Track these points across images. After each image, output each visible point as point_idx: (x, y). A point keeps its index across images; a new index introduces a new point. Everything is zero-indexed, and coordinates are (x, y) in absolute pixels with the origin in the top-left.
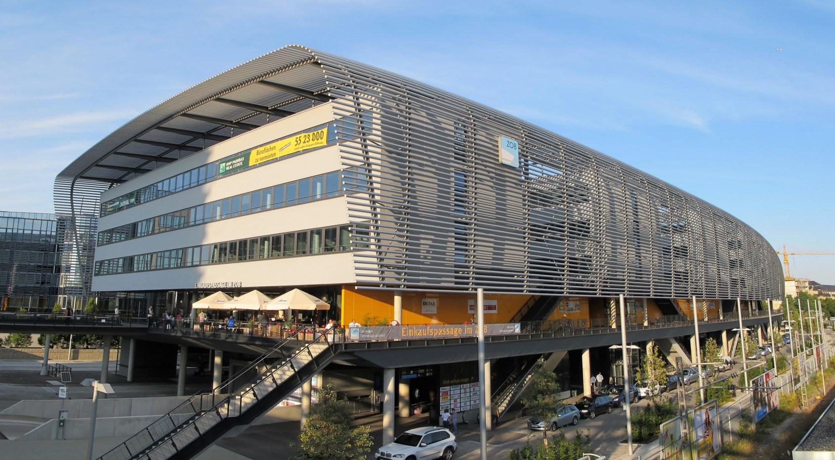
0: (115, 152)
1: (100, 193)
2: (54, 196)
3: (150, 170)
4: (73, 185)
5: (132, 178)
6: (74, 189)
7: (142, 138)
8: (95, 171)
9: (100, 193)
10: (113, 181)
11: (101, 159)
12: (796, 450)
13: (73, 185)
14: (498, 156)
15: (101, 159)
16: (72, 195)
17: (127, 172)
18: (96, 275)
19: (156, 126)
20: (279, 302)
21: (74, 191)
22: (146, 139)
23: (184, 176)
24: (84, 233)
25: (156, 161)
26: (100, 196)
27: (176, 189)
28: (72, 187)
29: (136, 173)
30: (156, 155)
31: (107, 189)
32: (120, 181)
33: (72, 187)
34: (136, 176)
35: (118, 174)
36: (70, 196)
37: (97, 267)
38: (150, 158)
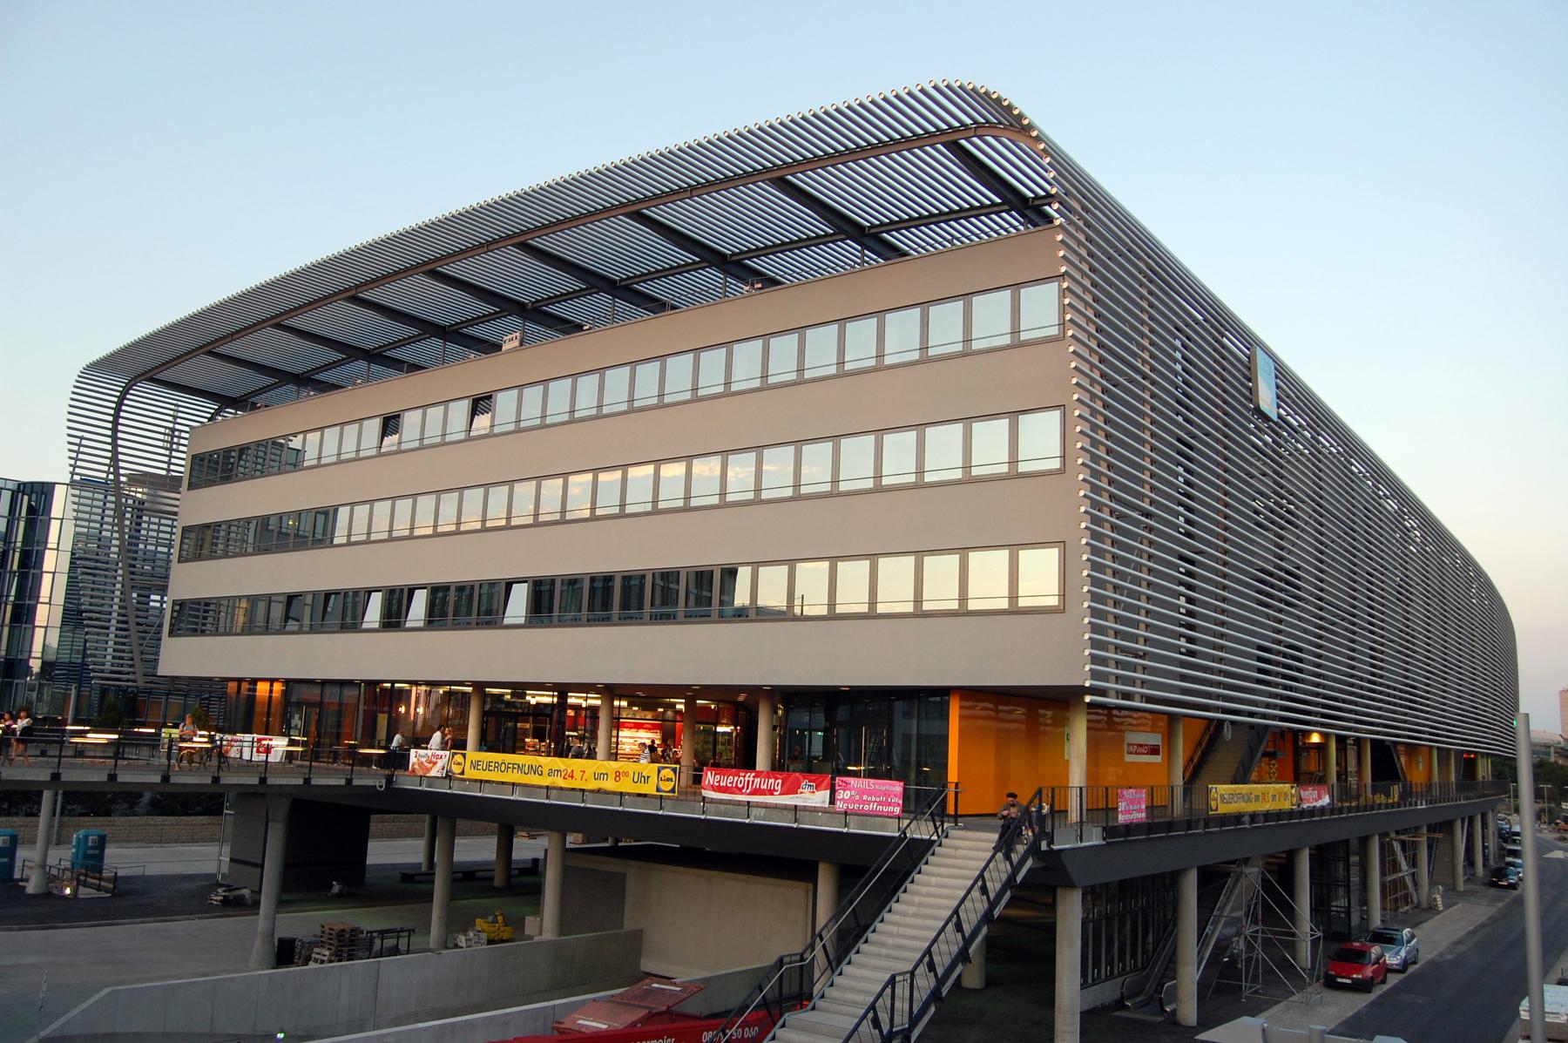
0: (210, 350)
1: (187, 429)
2: (69, 420)
3: (341, 387)
4: (122, 398)
5: (706, 297)
6: (114, 405)
7: (228, 349)
8: (206, 371)
10: (225, 401)
13: (122, 398)
14: (76, 526)
16: (115, 423)
18: (171, 633)
19: (145, 377)
20: (821, 992)
22: (238, 355)
23: (322, 435)
24: (86, 530)
25: (525, 318)
27: (444, 435)
28: (120, 404)
29: (445, 340)
30: (367, 347)
31: (206, 420)
32: (242, 403)
33: (120, 404)
34: (368, 379)
35: (243, 381)
36: (111, 418)
37: (245, 686)
38: (284, 377)
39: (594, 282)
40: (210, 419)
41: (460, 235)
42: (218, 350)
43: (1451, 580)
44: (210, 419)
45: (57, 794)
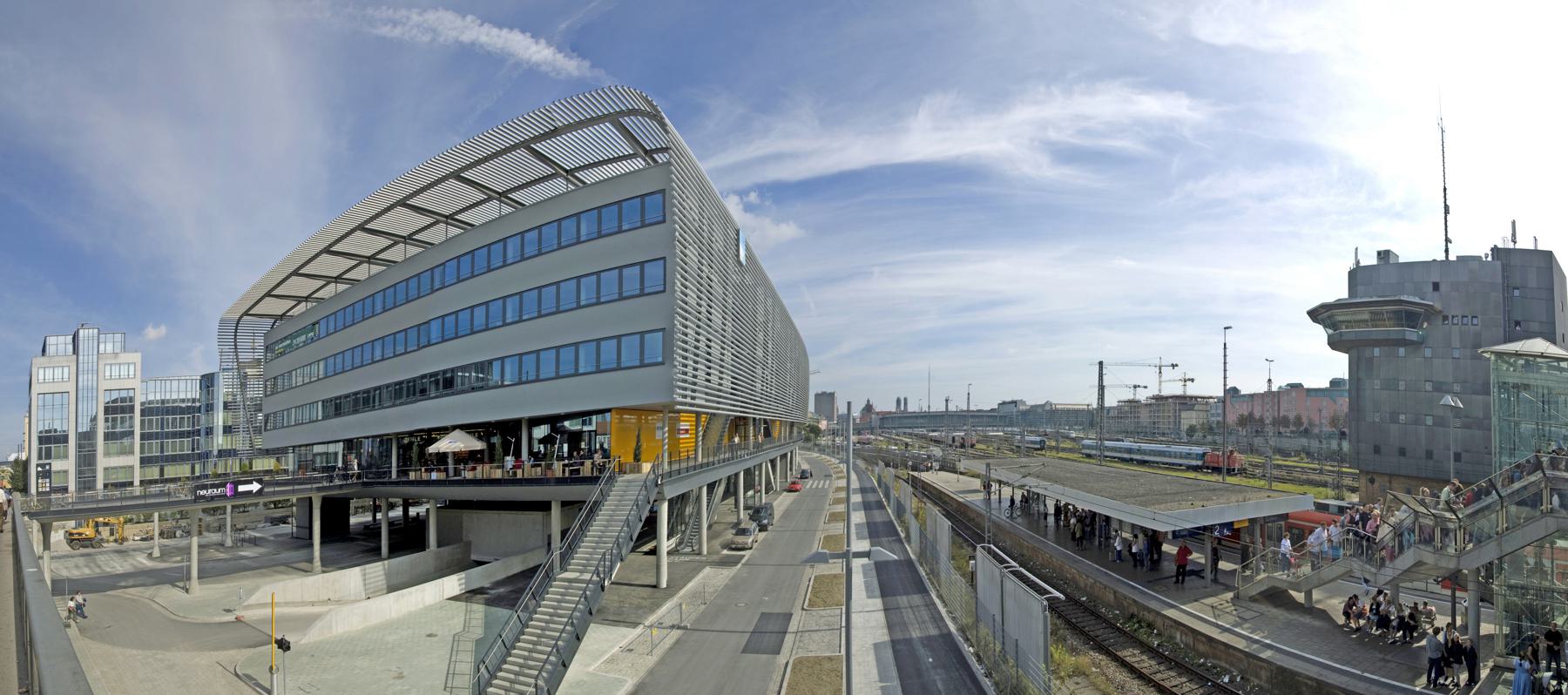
11: (278, 285)
15: (278, 285)
30: (335, 275)
41: (692, 190)
45: (157, 403)
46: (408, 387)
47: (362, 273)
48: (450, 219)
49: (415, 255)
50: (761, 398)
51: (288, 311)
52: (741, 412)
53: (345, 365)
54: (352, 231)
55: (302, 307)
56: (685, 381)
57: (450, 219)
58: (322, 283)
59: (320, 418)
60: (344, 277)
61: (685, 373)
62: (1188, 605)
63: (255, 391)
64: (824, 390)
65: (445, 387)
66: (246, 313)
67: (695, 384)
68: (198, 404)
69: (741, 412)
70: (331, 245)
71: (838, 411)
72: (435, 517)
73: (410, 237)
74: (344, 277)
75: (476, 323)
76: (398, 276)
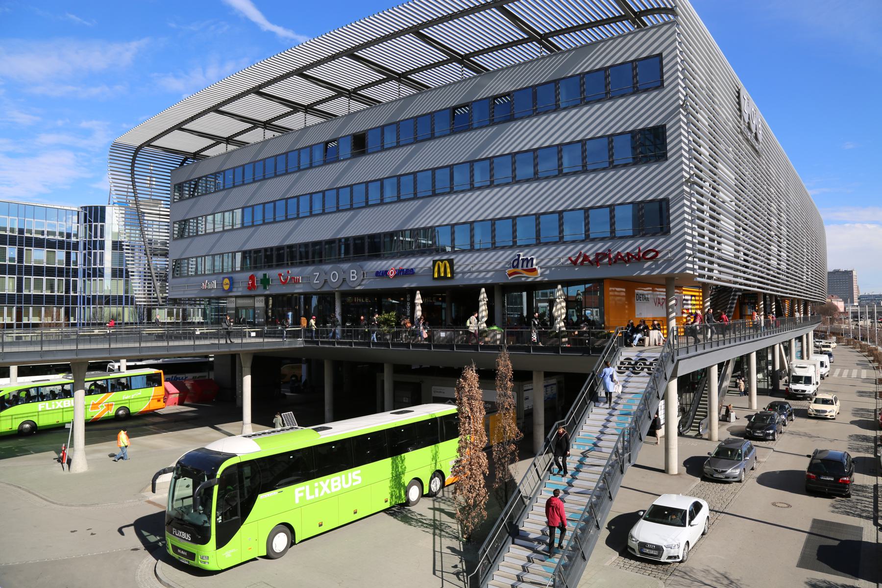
1: (169, 171)
9: (169, 171)
11: (192, 119)
12: (313, 429)
15: (192, 119)
17: (323, 120)
21: (135, 169)
26: (169, 175)
39: (390, 75)
40: (180, 165)
42: (152, 144)
43: (469, 139)
44: (180, 165)
46: (307, 258)
47: (296, 121)
48: (402, 78)
49: (358, 112)
50: (788, 277)
51: (557, 33)
52: (759, 287)
53: (289, 213)
54: (333, 57)
55: (221, 148)
56: (703, 252)
57: (402, 78)
58: (212, 142)
59: (238, 269)
60: (317, 107)
61: (703, 244)
62: (588, 395)
63: (158, 233)
64: (837, 268)
65: (355, 252)
66: (148, 144)
67: (712, 255)
68: (74, 239)
69: (759, 287)
70: (261, 86)
71: (859, 293)
72: (733, 367)
73: (355, 91)
74: (317, 107)
75: (438, 185)
76: (245, 158)
